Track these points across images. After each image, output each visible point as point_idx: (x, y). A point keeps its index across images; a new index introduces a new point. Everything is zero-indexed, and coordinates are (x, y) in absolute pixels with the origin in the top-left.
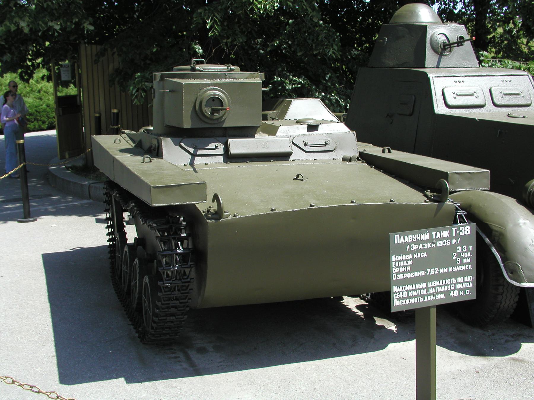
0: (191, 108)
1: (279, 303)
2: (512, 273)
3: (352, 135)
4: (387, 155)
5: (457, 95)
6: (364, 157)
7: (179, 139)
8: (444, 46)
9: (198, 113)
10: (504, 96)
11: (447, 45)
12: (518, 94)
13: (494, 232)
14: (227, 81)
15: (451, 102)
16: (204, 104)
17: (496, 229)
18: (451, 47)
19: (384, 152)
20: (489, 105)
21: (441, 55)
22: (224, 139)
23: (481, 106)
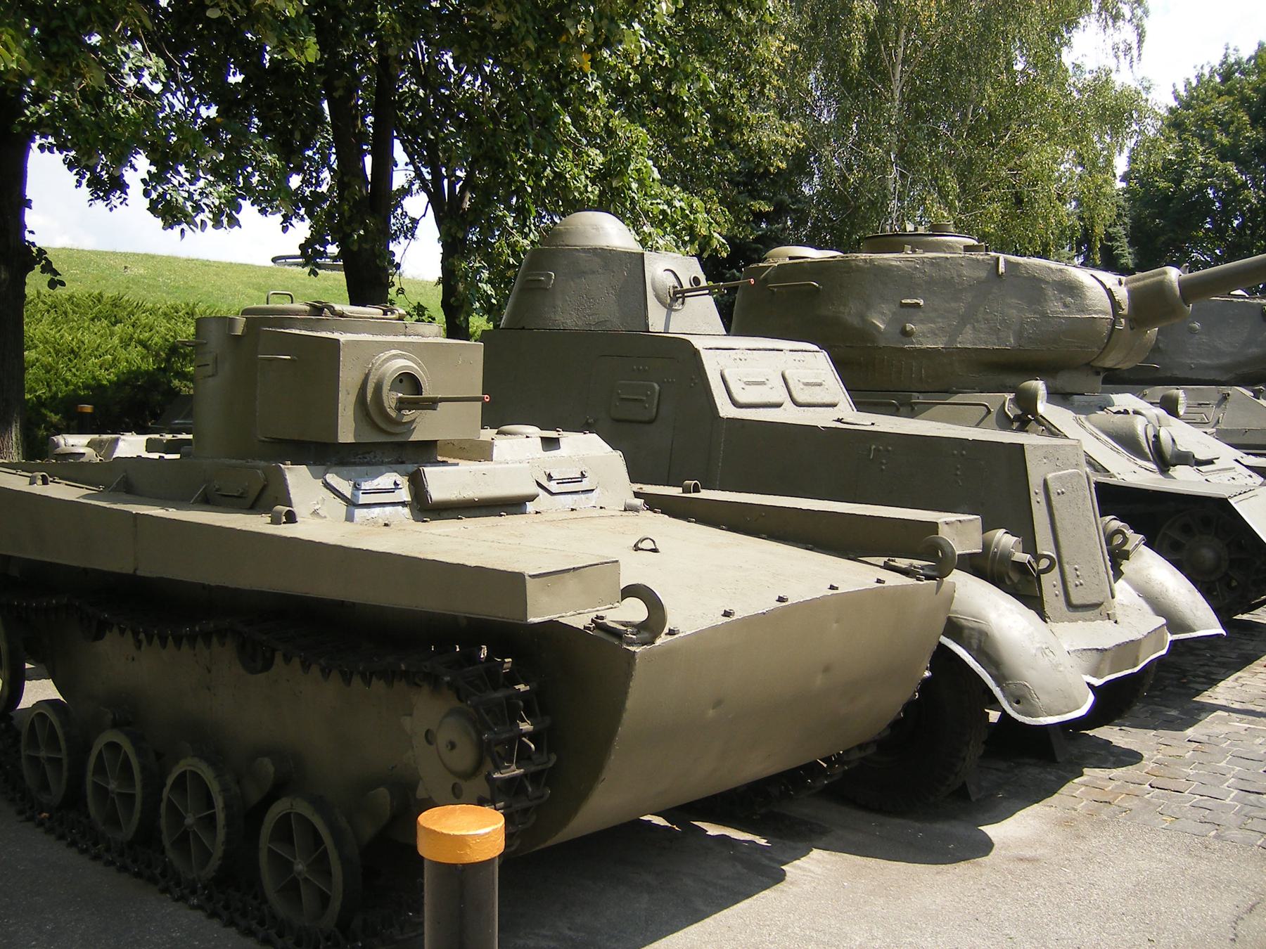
0: (352, 398)
1: (615, 827)
2: (1018, 702)
3: (616, 460)
4: (38, 489)
5: (748, 383)
6: (655, 504)
7: (321, 468)
8: (675, 293)
9: (369, 408)
10: (747, 387)
11: (679, 292)
12: (763, 383)
13: (966, 632)
14: (409, 339)
15: (741, 398)
16: (386, 388)
17: (969, 624)
18: (684, 298)
19: (31, 483)
20: (788, 404)
21: (670, 309)
22: (411, 468)
23: (779, 405)
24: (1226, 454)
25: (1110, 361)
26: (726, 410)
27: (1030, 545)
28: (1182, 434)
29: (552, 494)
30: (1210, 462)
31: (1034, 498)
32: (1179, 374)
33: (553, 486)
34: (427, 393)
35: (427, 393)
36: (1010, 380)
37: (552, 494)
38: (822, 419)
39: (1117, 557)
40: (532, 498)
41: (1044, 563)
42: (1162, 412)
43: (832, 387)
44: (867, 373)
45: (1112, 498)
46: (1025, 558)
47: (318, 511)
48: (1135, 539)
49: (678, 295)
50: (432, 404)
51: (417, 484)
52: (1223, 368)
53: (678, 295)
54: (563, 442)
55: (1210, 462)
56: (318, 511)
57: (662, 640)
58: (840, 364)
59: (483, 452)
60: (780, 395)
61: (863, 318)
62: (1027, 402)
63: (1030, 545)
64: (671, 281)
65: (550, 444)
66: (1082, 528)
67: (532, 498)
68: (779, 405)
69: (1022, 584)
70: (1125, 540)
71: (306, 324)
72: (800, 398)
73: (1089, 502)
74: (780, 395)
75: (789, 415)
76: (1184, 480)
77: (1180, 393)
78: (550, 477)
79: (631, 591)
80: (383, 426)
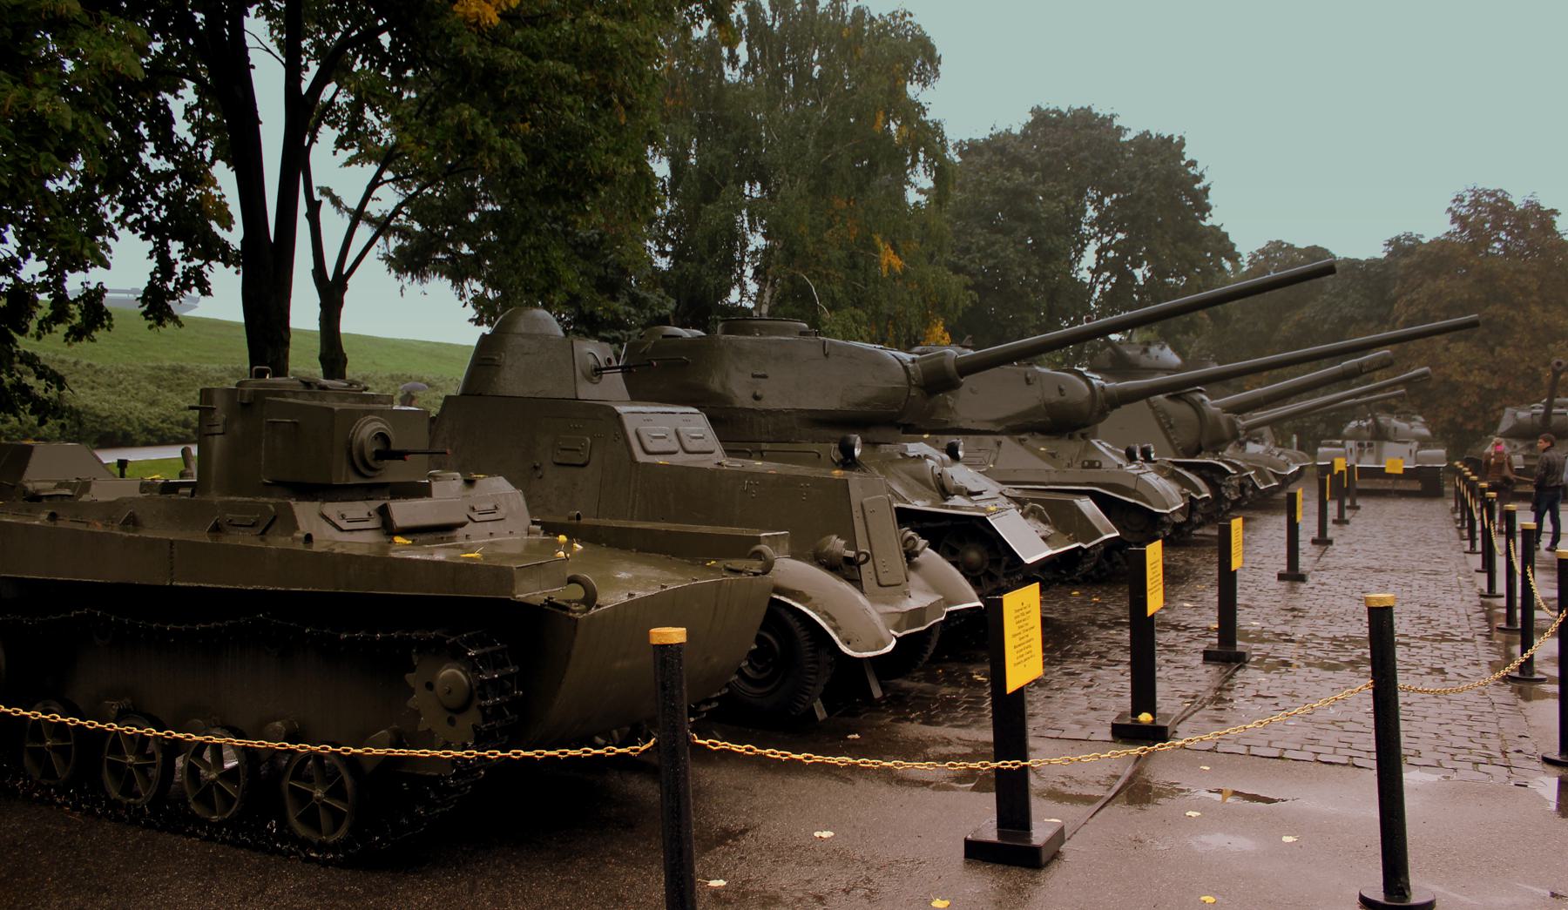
15: (651, 448)
20: (681, 453)
23: (674, 453)
24: (991, 488)
25: (905, 420)
26: (641, 457)
27: (852, 544)
28: (961, 474)
29: (341, 530)
30: (980, 493)
31: (855, 515)
32: (964, 425)
33: (344, 525)
34: (394, 447)
35: (394, 447)
36: (839, 434)
37: (341, 530)
38: (708, 463)
39: (910, 555)
40: (462, 525)
41: (863, 557)
42: (946, 457)
43: (711, 440)
44: (732, 425)
45: (906, 517)
46: (851, 554)
47: (336, 529)
48: (922, 542)
49: (598, 371)
50: (401, 455)
51: (384, 512)
52: (998, 421)
53: (598, 371)
54: (436, 487)
55: (980, 493)
56: (336, 529)
57: (593, 610)
58: (713, 420)
59: (423, 491)
60: (675, 446)
61: (723, 386)
62: (847, 450)
63: (852, 544)
64: (591, 361)
65: (470, 483)
66: (888, 539)
67: (462, 525)
68: (674, 453)
69: (846, 569)
70: (916, 544)
71: (295, 394)
72: (689, 447)
73: (891, 520)
74: (675, 446)
75: (680, 459)
76: (959, 505)
77: (960, 441)
78: (343, 517)
79: (572, 580)
80: (363, 470)
